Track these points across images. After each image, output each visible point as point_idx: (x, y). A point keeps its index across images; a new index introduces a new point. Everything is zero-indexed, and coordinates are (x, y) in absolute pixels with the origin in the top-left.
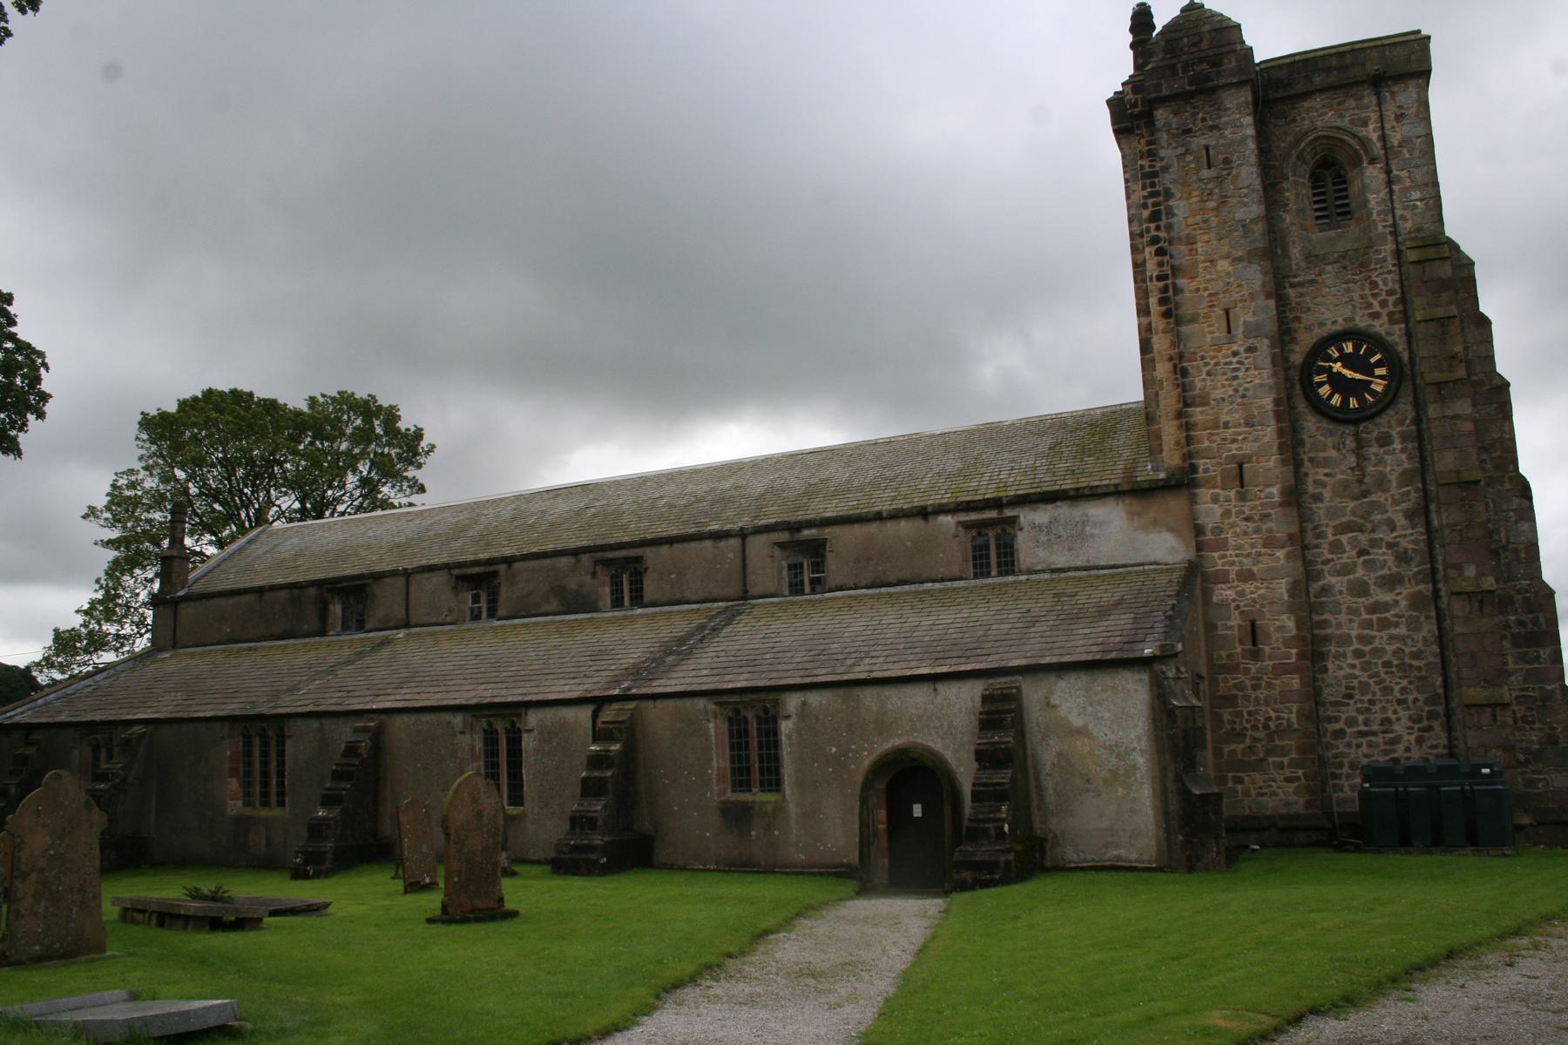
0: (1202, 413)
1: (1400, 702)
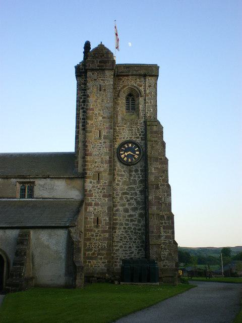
1: (134, 242)
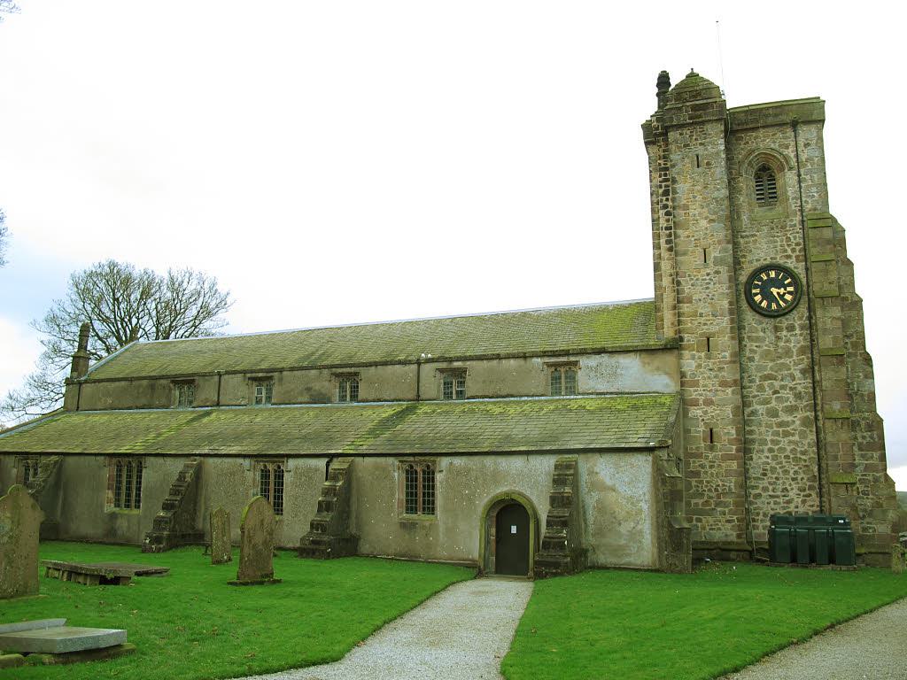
0: (687, 307)
1: (793, 479)
